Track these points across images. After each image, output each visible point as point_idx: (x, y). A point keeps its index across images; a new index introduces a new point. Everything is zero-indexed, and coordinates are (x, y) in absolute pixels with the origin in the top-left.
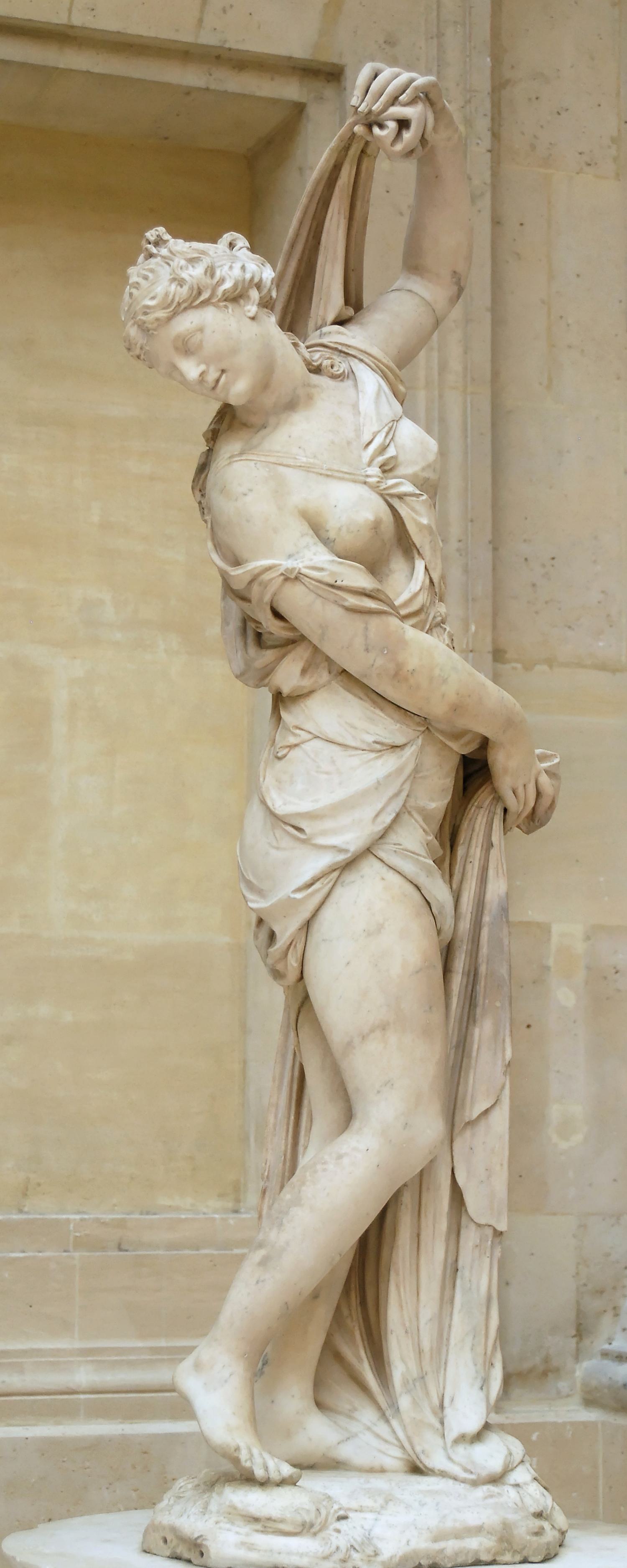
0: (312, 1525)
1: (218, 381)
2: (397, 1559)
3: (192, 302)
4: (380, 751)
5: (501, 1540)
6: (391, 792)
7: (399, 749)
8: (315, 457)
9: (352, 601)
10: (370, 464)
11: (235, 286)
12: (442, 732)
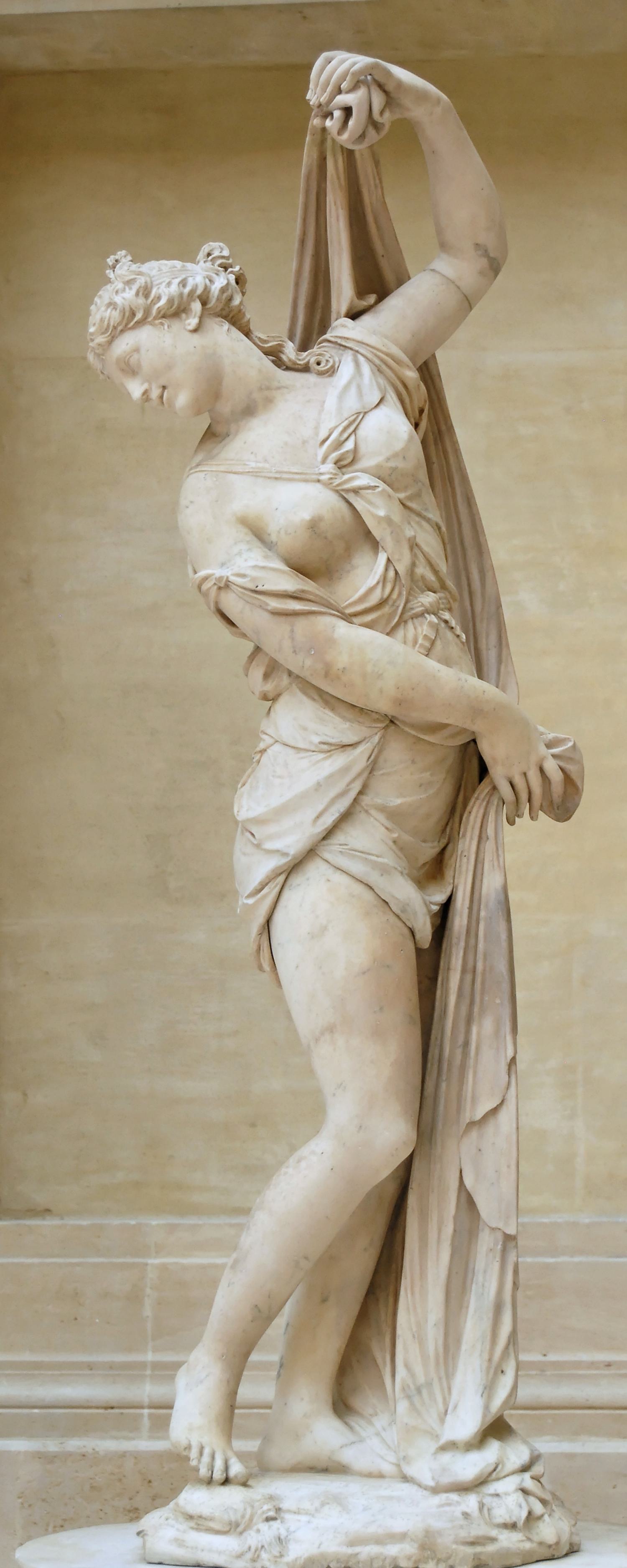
0: (237, 1525)
1: (161, 397)
2: (302, 1561)
3: (126, 325)
4: (329, 751)
5: (423, 1547)
6: (333, 793)
7: (350, 748)
8: (266, 461)
9: (275, 604)
10: (324, 461)
11: (171, 301)
12: (413, 726)
